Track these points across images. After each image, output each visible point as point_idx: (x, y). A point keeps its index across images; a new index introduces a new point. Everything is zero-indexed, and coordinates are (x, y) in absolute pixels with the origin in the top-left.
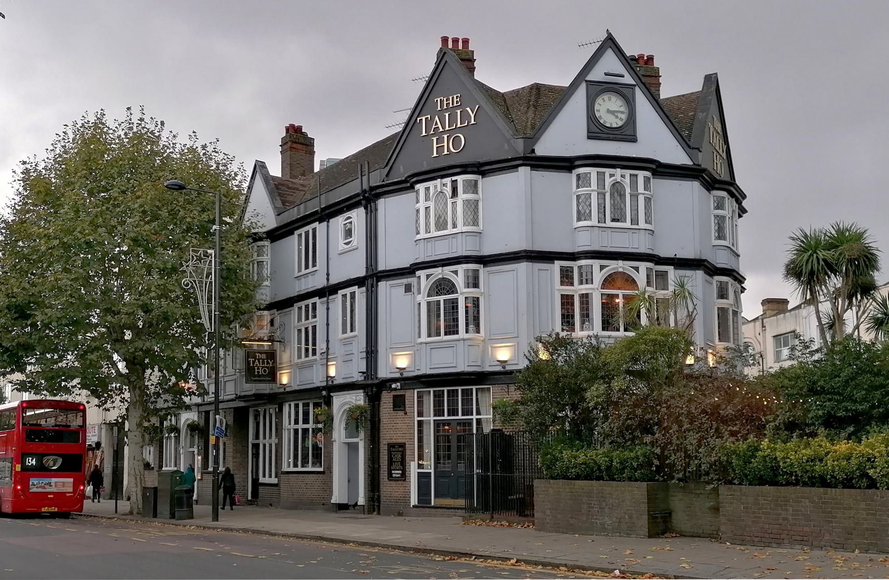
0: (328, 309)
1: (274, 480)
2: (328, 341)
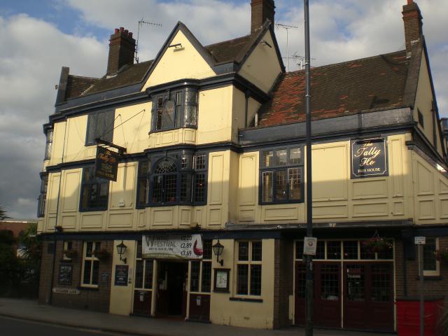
1: (96, 286)
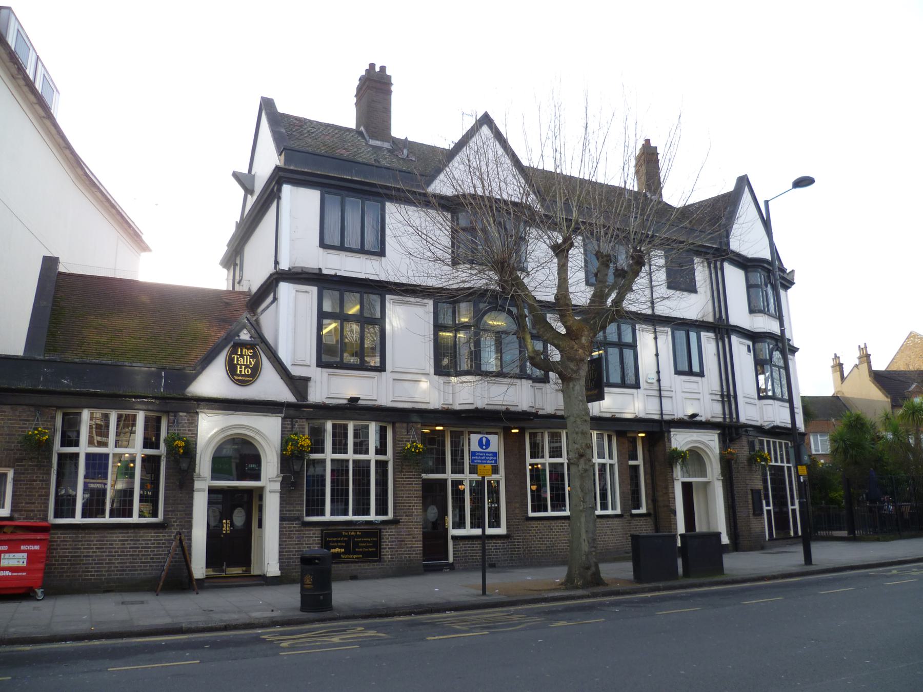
0: (656, 338)
2: (658, 372)
